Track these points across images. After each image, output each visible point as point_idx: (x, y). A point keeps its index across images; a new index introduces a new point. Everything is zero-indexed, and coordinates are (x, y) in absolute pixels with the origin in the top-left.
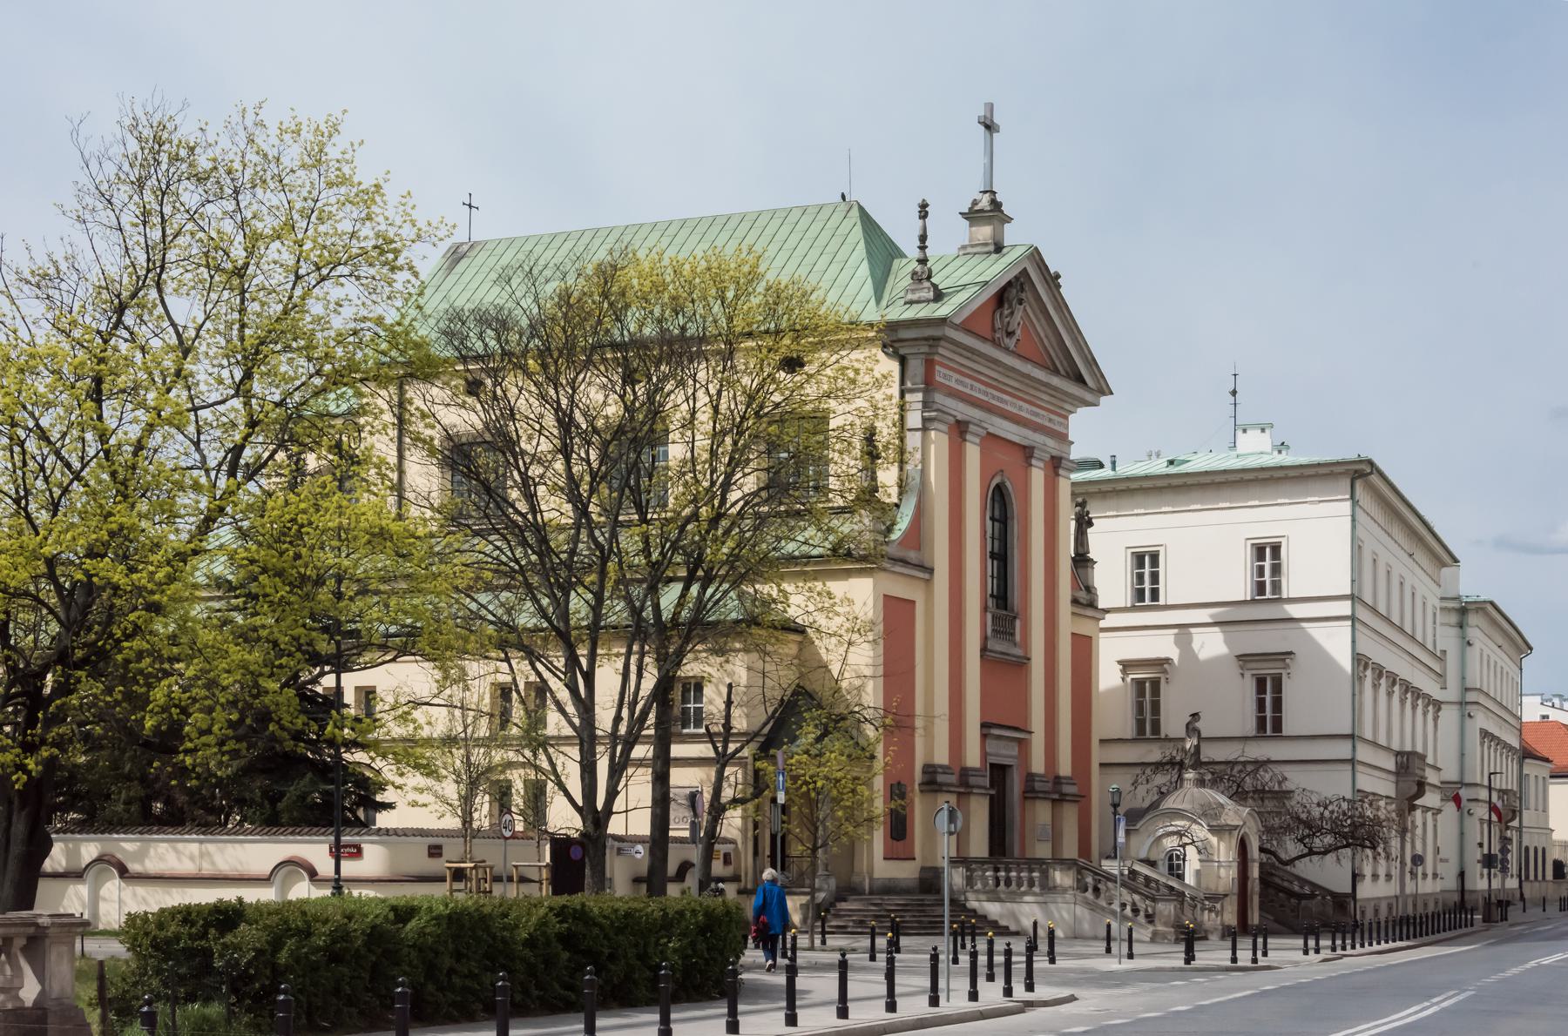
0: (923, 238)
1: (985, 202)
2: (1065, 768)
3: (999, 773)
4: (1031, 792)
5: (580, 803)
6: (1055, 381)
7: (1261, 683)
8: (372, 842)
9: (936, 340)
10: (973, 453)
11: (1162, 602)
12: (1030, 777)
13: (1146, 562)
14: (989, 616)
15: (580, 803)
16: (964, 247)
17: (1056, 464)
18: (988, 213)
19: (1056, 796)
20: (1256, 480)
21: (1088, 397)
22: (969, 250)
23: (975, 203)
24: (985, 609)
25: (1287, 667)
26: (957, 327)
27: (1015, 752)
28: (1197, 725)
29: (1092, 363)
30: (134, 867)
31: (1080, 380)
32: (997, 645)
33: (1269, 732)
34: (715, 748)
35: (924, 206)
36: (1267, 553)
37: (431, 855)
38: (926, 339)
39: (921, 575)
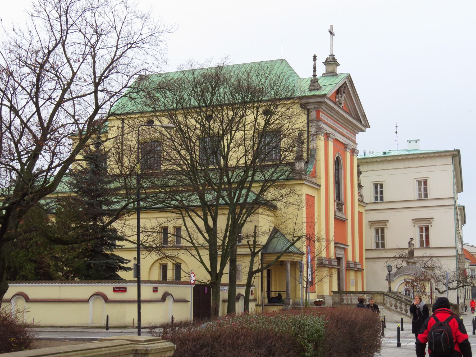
0: (315, 68)
1: (331, 59)
2: (357, 260)
3: (339, 259)
4: (348, 268)
5: (210, 270)
6: (354, 122)
7: (421, 228)
8: (131, 286)
9: (321, 103)
10: (331, 144)
11: (384, 201)
12: (348, 263)
13: (379, 188)
14: (336, 203)
15: (210, 270)
16: (324, 74)
17: (354, 151)
18: (331, 62)
19: (356, 269)
20: (418, 158)
21: (363, 128)
22: (326, 75)
23: (327, 59)
24: (335, 201)
25: (431, 223)
26: (328, 98)
27: (343, 253)
28: (412, 242)
29: (364, 116)
30: (31, 297)
31: (360, 121)
32: (339, 214)
33: (425, 246)
34: (251, 250)
35: (315, 57)
36: (423, 184)
37: (154, 291)
38: (318, 102)
39: (317, 187)
